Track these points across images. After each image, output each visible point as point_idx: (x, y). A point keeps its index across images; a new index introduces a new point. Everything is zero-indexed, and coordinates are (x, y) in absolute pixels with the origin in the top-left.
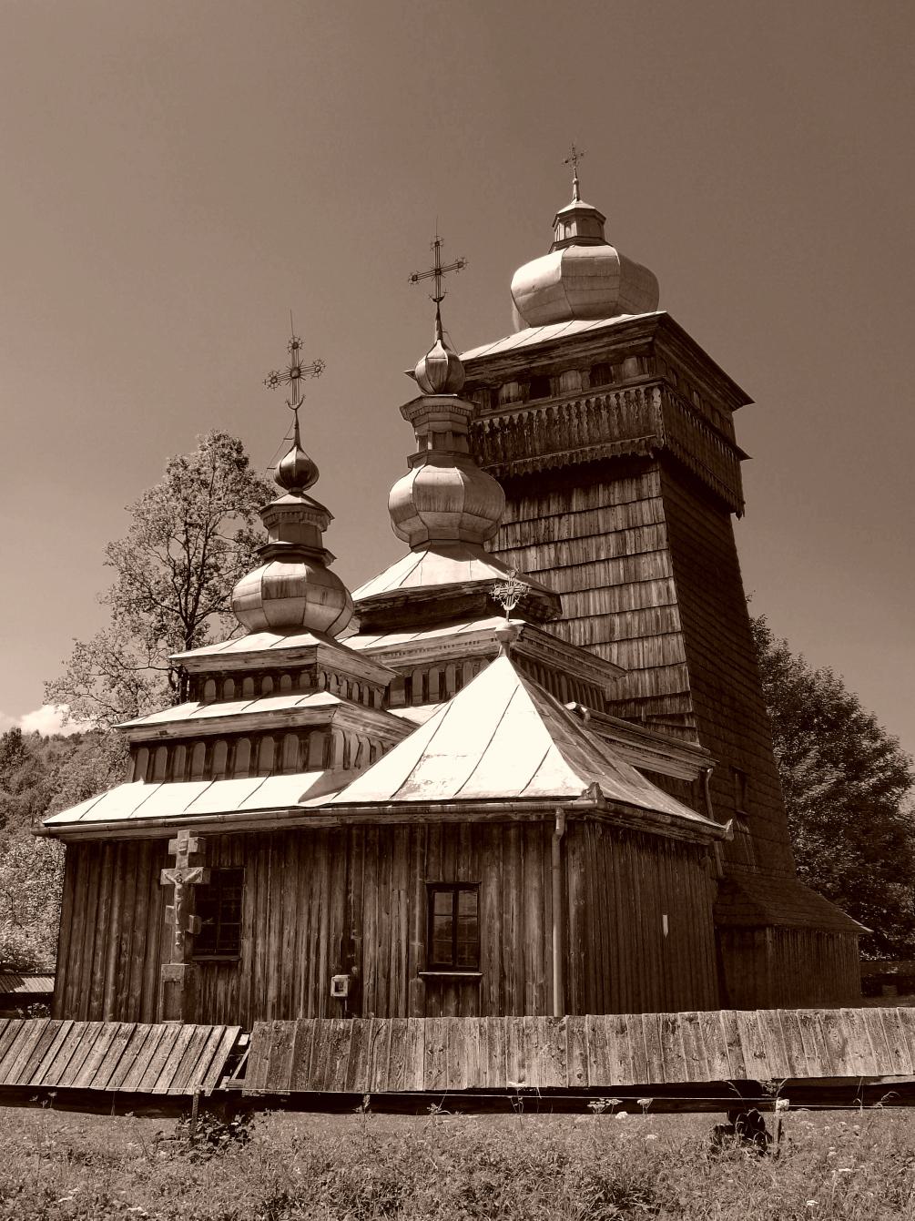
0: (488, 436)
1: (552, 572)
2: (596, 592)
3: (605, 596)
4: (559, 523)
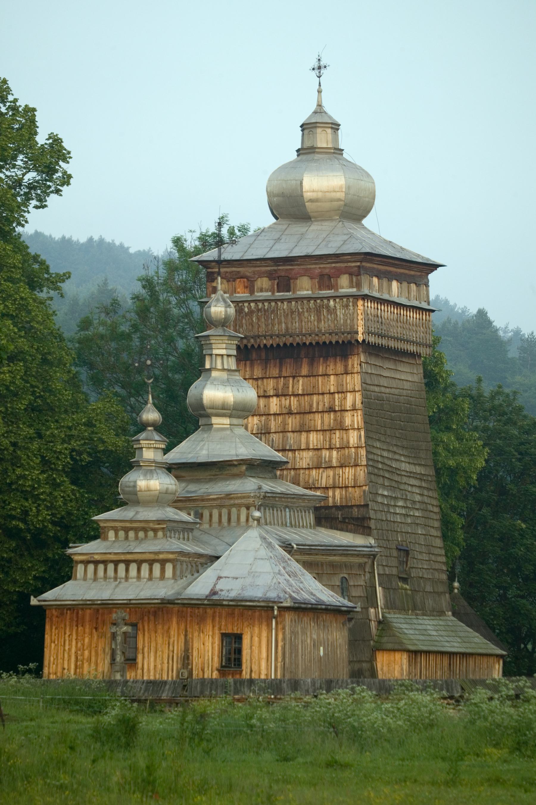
0: (246, 314)
1: (287, 416)
2: (315, 433)
3: (320, 436)
4: (293, 382)
